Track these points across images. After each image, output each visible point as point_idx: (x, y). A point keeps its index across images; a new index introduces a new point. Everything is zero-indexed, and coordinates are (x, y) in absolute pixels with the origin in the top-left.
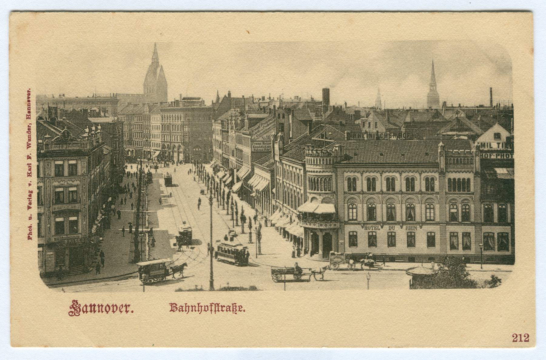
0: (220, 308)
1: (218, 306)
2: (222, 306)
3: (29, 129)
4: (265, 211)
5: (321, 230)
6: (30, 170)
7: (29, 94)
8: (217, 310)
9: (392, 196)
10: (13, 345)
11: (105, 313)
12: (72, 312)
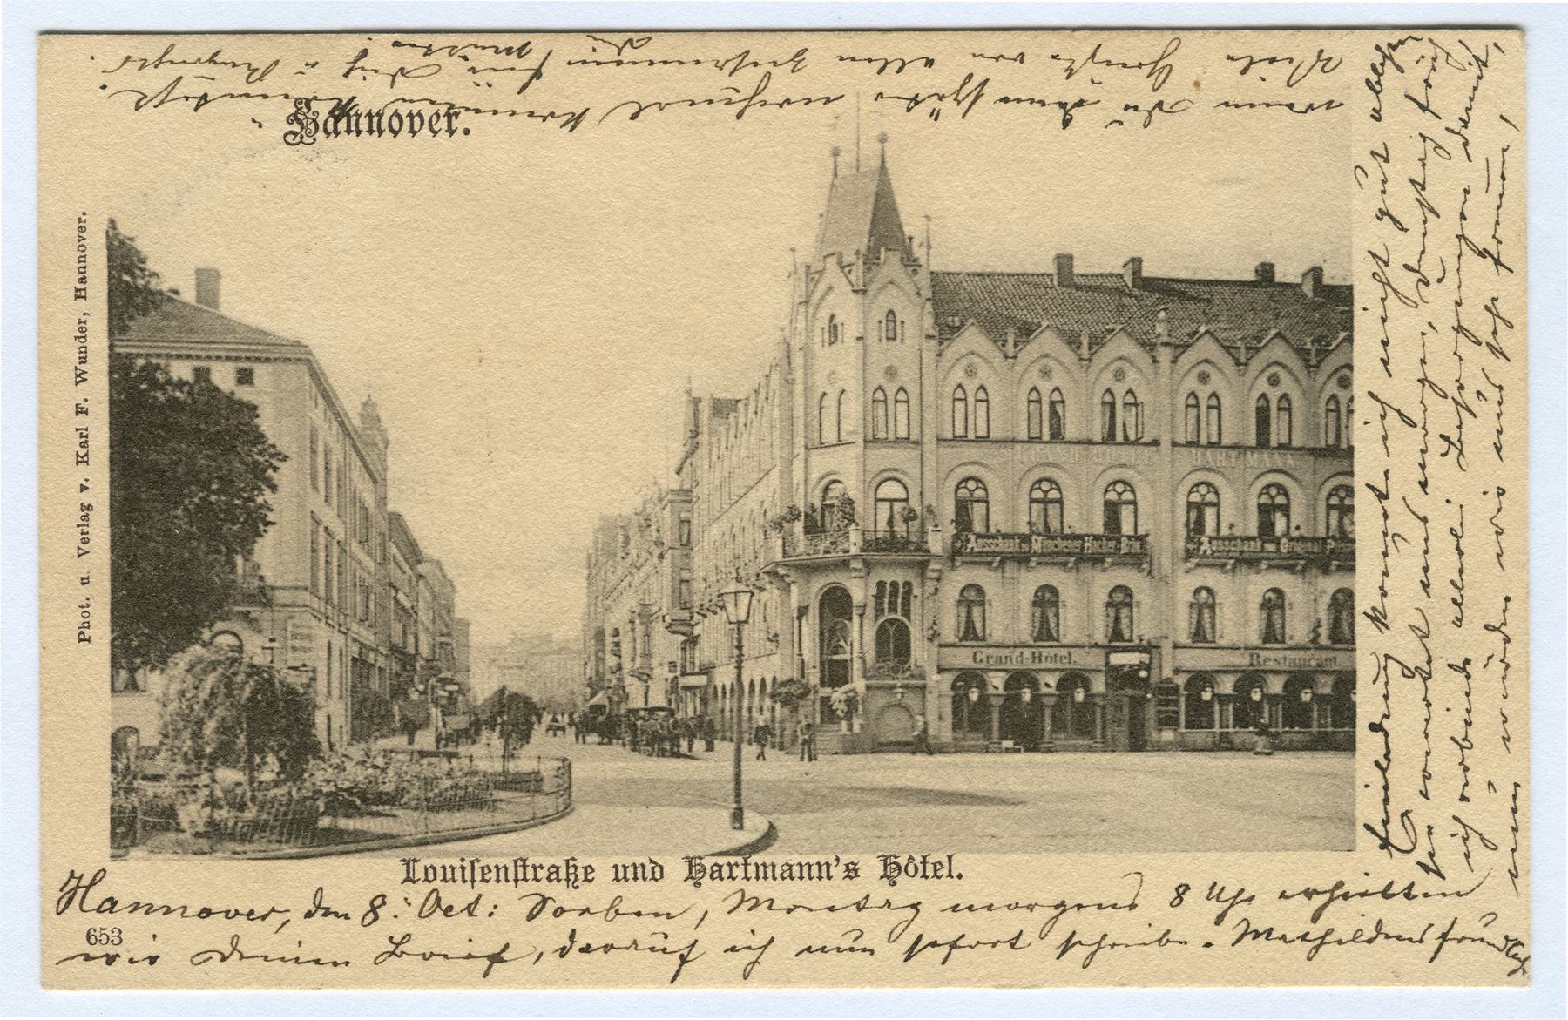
0: (530, 872)
1: (524, 866)
2: (534, 868)
3: (81, 330)
6: (84, 445)
7: (82, 229)
8: (520, 876)
10: (44, 985)
11: (387, 134)
12: (295, 133)
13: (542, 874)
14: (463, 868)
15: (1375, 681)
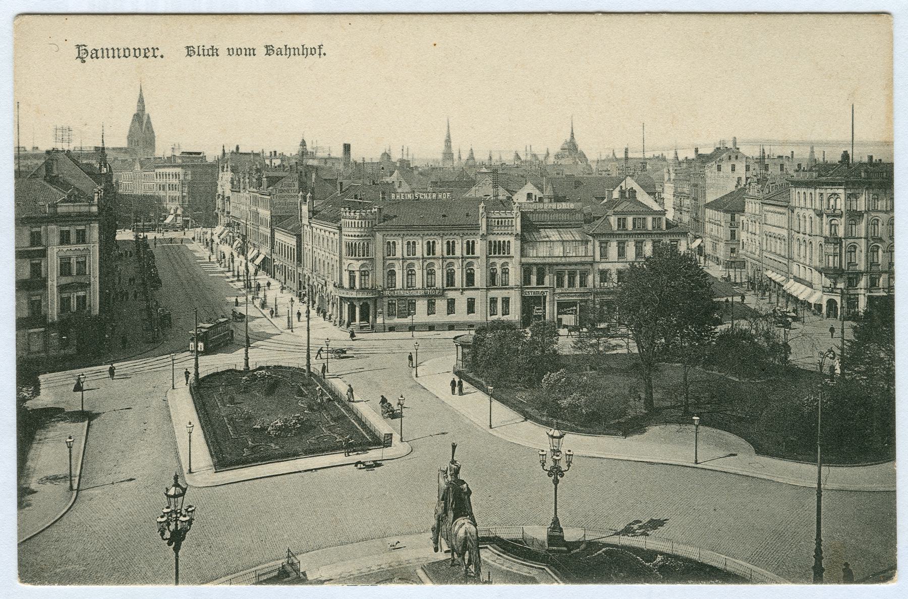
4: (288, 281)
5: (359, 299)
9: (432, 261)
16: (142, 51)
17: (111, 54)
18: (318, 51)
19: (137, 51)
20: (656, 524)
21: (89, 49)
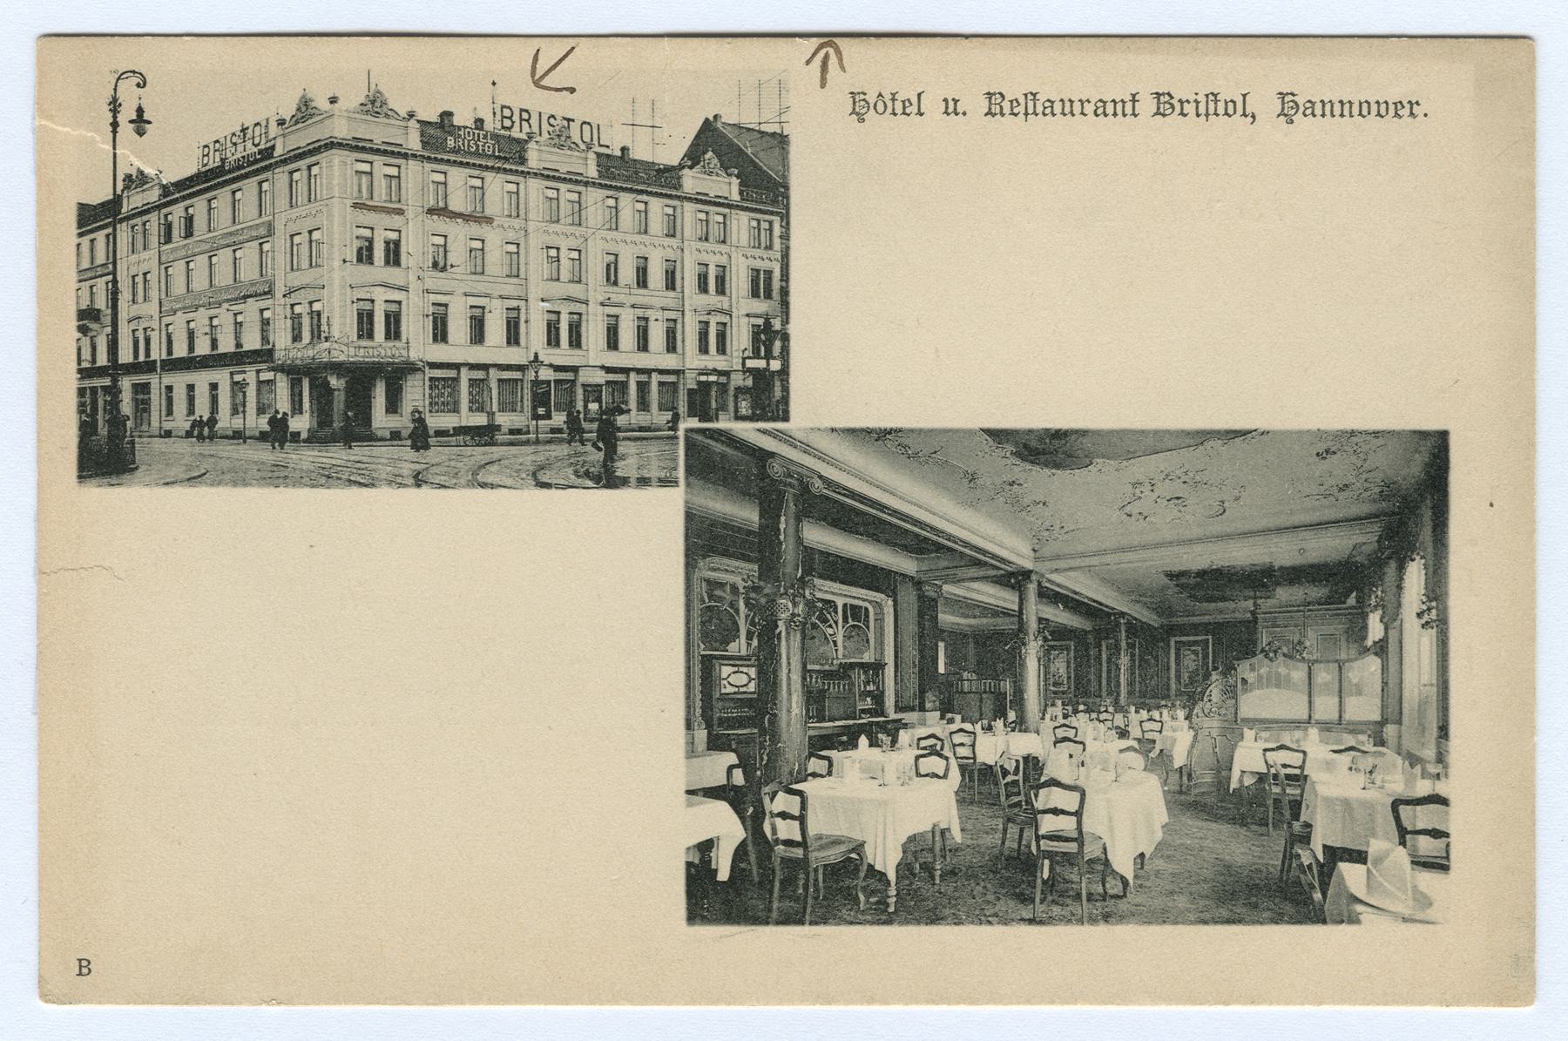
1: (1034, 100)
8: (1211, 111)
13: (1089, 108)
14: (1197, 102)
15: (808, 62)
16: (1392, 107)
17: (1337, 110)
18: (1406, 108)
19: (1383, 107)
20: (843, 68)
21: (1300, 100)
